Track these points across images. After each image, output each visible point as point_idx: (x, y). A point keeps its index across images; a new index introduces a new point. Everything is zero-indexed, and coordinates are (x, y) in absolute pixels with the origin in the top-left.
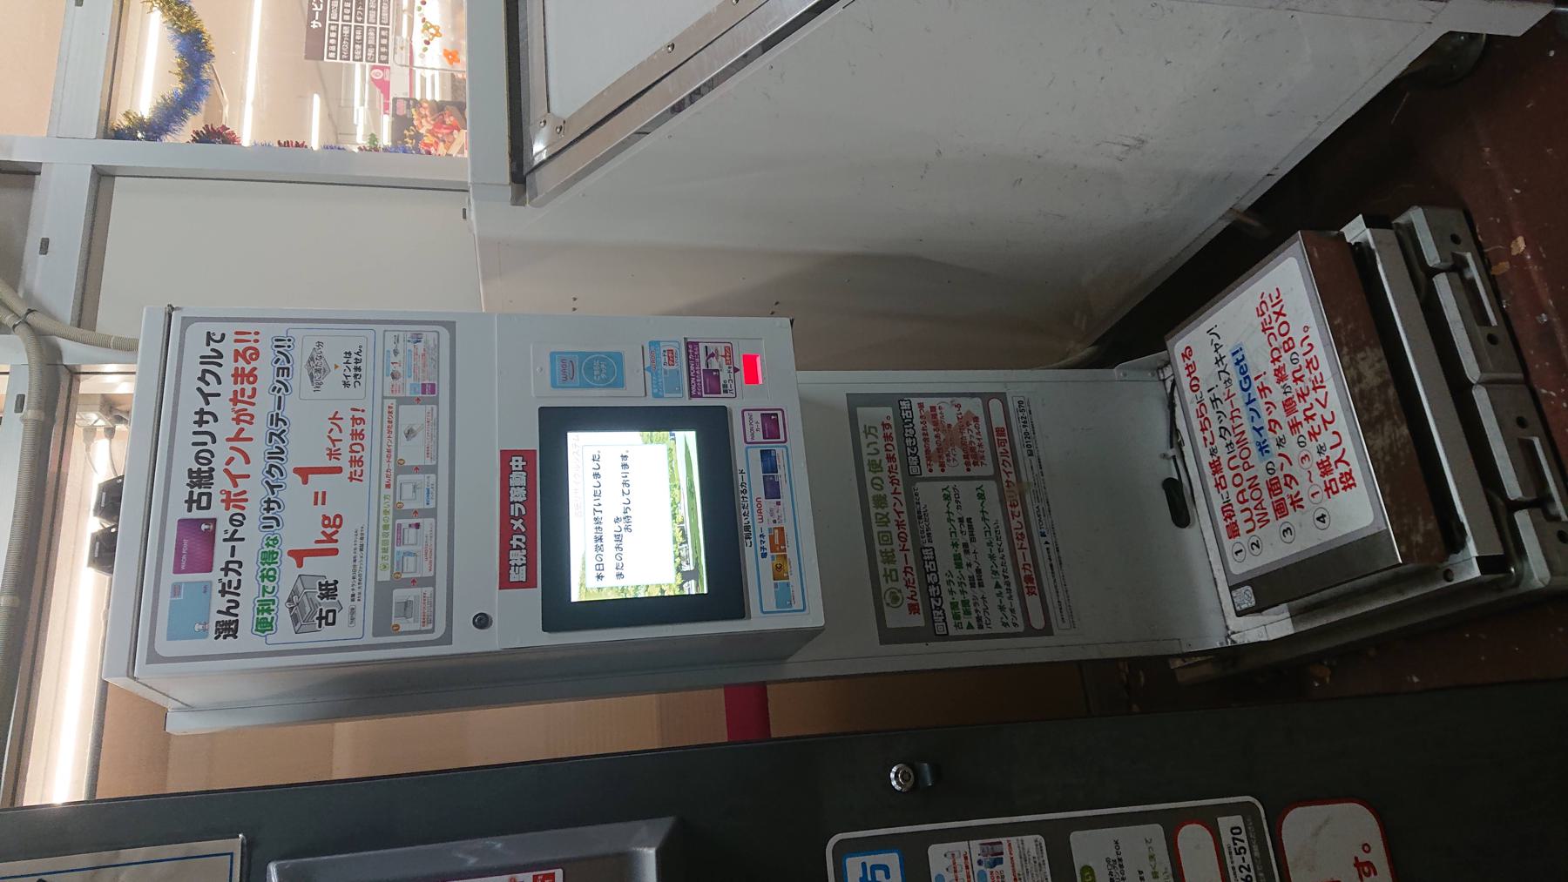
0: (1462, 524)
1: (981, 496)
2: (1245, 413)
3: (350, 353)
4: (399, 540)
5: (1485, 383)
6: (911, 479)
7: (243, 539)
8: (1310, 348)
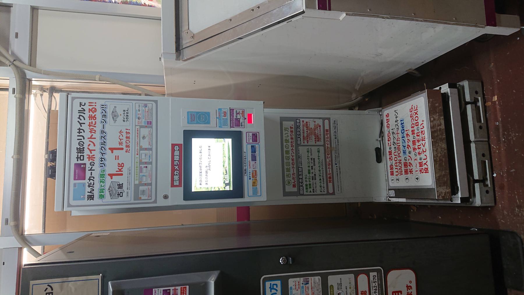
0: (458, 187)
1: (319, 151)
2: (401, 139)
3: (125, 110)
4: (141, 171)
5: (475, 142)
6: (298, 145)
7: (94, 170)
8: (423, 127)
